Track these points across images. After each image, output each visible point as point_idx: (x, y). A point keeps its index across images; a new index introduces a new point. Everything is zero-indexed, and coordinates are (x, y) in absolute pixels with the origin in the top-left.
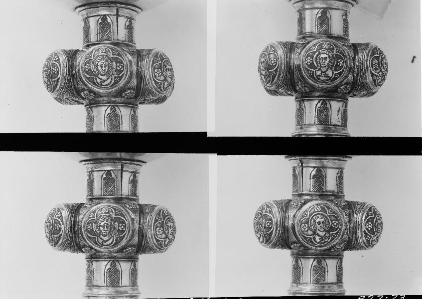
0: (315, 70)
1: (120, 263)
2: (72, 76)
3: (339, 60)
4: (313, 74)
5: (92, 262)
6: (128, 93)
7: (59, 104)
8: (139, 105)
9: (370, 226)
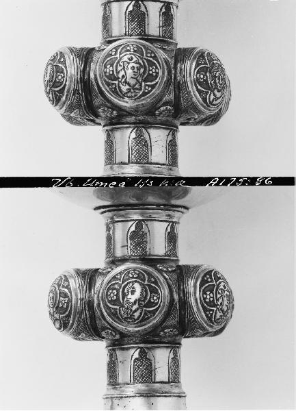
0: (117, 82)
1: (117, 352)
2: (85, 84)
3: (151, 68)
4: (115, 88)
5: (114, 350)
6: (163, 111)
7: (68, 124)
8: (180, 127)
9: (208, 297)
